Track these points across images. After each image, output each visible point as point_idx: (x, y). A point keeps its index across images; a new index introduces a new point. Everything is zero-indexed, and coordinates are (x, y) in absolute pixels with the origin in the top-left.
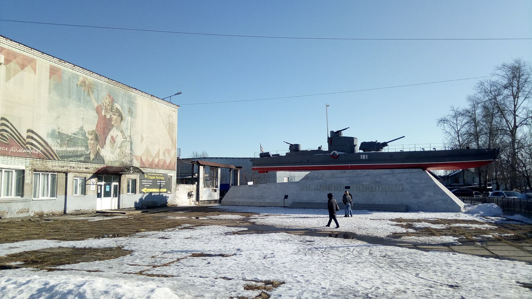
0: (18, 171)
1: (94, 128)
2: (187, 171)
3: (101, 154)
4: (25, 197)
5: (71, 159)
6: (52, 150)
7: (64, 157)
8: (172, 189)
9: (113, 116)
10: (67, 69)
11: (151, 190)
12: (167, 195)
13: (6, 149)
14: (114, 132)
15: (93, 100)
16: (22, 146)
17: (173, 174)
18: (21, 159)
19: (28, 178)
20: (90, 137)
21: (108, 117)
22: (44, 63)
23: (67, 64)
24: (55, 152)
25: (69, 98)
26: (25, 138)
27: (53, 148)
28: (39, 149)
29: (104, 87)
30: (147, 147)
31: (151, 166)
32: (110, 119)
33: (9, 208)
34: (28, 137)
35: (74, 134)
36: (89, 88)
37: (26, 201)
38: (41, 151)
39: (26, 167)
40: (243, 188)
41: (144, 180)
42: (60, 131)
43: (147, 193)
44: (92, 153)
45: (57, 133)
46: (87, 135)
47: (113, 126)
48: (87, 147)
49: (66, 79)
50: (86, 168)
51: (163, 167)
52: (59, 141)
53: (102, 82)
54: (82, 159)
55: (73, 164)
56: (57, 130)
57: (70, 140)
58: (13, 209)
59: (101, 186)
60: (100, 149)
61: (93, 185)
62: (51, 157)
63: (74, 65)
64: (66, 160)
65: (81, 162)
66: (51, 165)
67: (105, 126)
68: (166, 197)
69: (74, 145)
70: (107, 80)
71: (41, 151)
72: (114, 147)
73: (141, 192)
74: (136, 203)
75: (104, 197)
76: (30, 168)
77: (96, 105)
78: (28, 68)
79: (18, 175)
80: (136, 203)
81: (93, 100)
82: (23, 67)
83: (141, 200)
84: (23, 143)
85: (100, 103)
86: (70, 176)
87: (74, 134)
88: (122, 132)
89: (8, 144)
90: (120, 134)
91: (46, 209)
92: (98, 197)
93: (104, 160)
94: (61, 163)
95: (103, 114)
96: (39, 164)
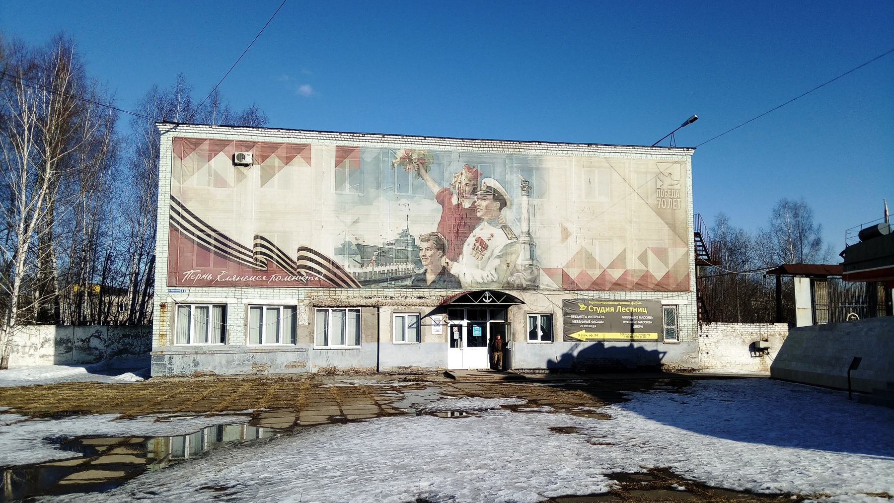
0: (216, 306)
1: (434, 229)
2: (726, 294)
3: (452, 272)
4: (298, 345)
5: (385, 284)
6: (345, 273)
7: (366, 283)
8: (681, 333)
9: (478, 202)
10: (370, 145)
11: (600, 336)
12: (661, 347)
13: (264, 278)
14: (482, 231)
15: (430, 184)
16: (291, 272)
17: (687, 304)
18: (289, 291)
19: (303, 318)
20: (424, 245)
21: (467, 205)
22: (324, 147)
23: (368, 137)
24: (351, 275)
25: (378, 188)
26: (295, 259)
27: (347, 270)
28: (319, 273)
29: (454, 156)
30: (625, 250)
31: (597, 285)
32: (473, 209)
33: (273, 361)
34: (299, 258)
35: (388, 244)
36: (422, 164)
37: (300, 350)
38: (325, 276)
39: (300, 301)
40: (504, 407)
41: (576, 314)
42: (360, 242)
43: (587, 340)
44: (429, 271)
45: (354, 247)
46: (417, 243)
47: (480, 220)
48: (418, 262)
49: (369, 160)
50: (420, 298)
51: (640, 286)
52: (358, 258)
53: (452, 147)
54: (408, 282)
55: (390, 292)
56: (354, 242)
57: (382, 255)
58: (279, 362)
59: (460, 327)
60: (450, 263)
61: (437, 328)
62: (343, 284)
63: (384, 135)
64: (373, 286)
65: (407, 287)
66: (344, 295)
67: (459, 224)
68: (656, 353)
69: (390, 262)
70: (459, 142)
71: (325, 276)
72: (485, 258)
73: (567, 338)
74: (550, 362)
75: (469, 345)
76: (307, 302)
77: (436, 189)
78: (298, 159)
79: (218, 311)
80: (550, 362)
81: (430, 184)
82: (288, 160)
83: (566, 357)
84: (292, 267)
85: (446, 185)
86: (385, 312)
87: (388, 244)
88: (504, 227)
89: (266, 271)
90: (499, 233)
91: (341, 363)
92: (452, 346)
93: (459, 282)
94: (365, 292)
95: (455, 201)
96: (322, 295)
